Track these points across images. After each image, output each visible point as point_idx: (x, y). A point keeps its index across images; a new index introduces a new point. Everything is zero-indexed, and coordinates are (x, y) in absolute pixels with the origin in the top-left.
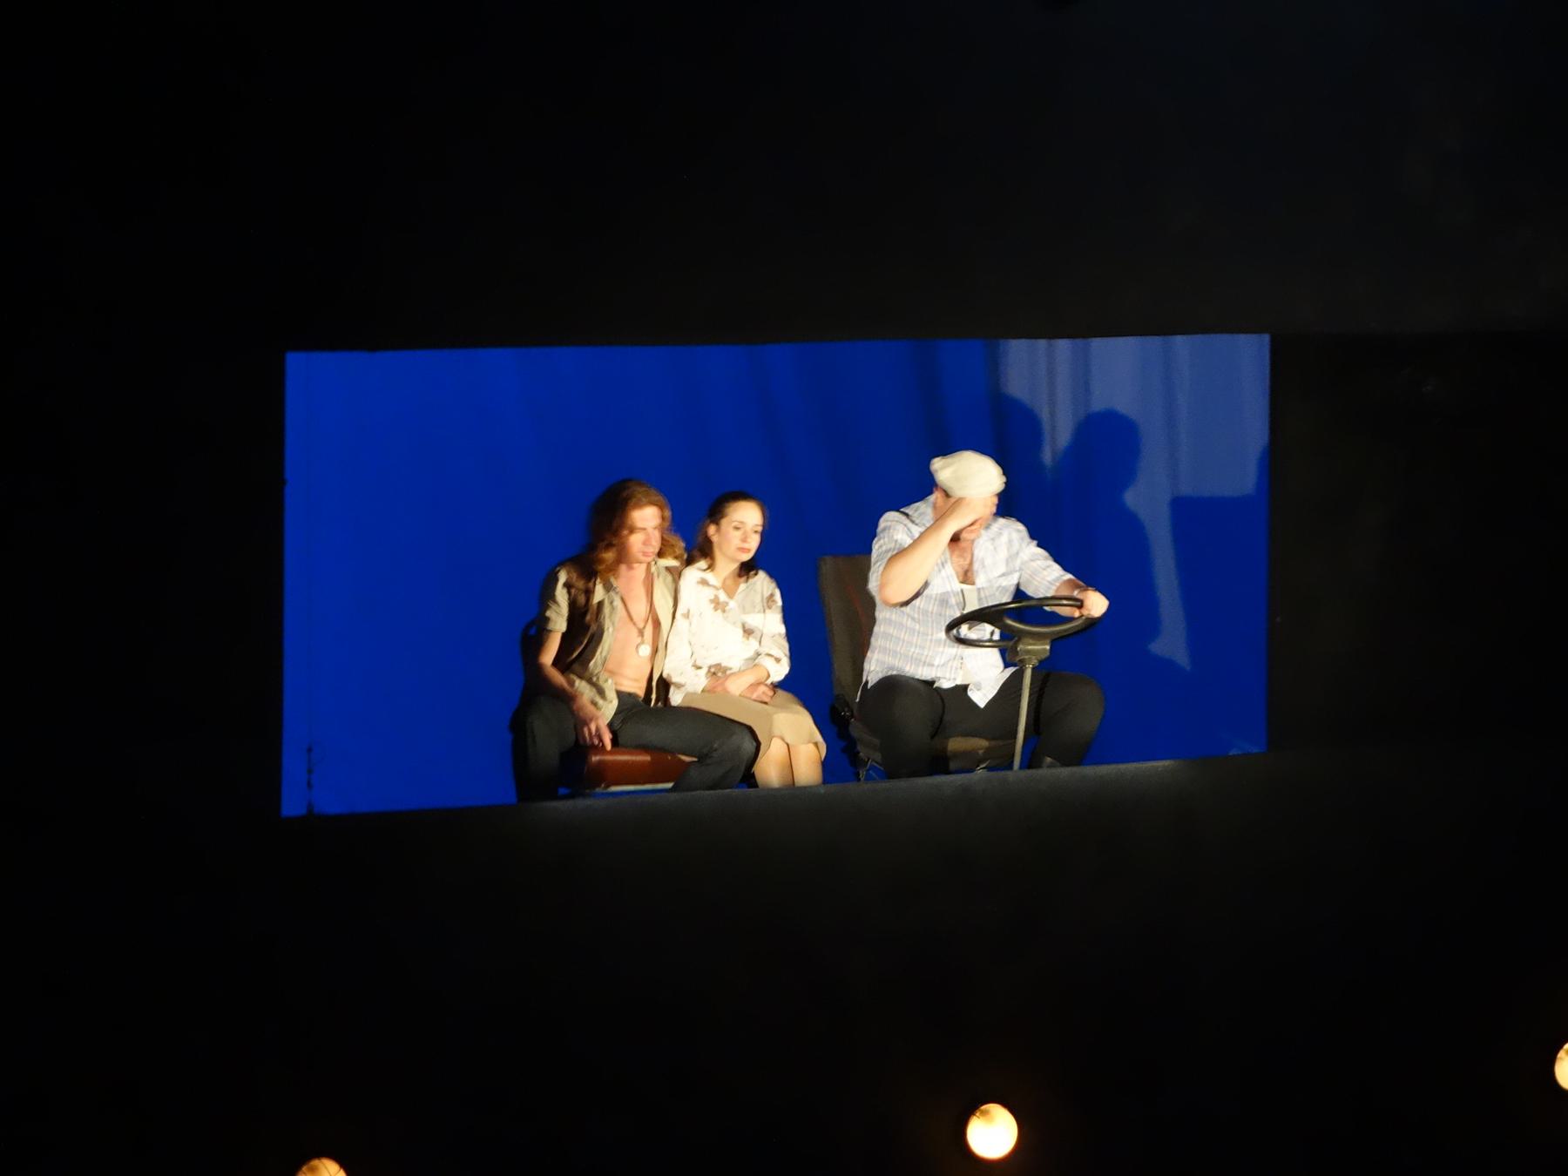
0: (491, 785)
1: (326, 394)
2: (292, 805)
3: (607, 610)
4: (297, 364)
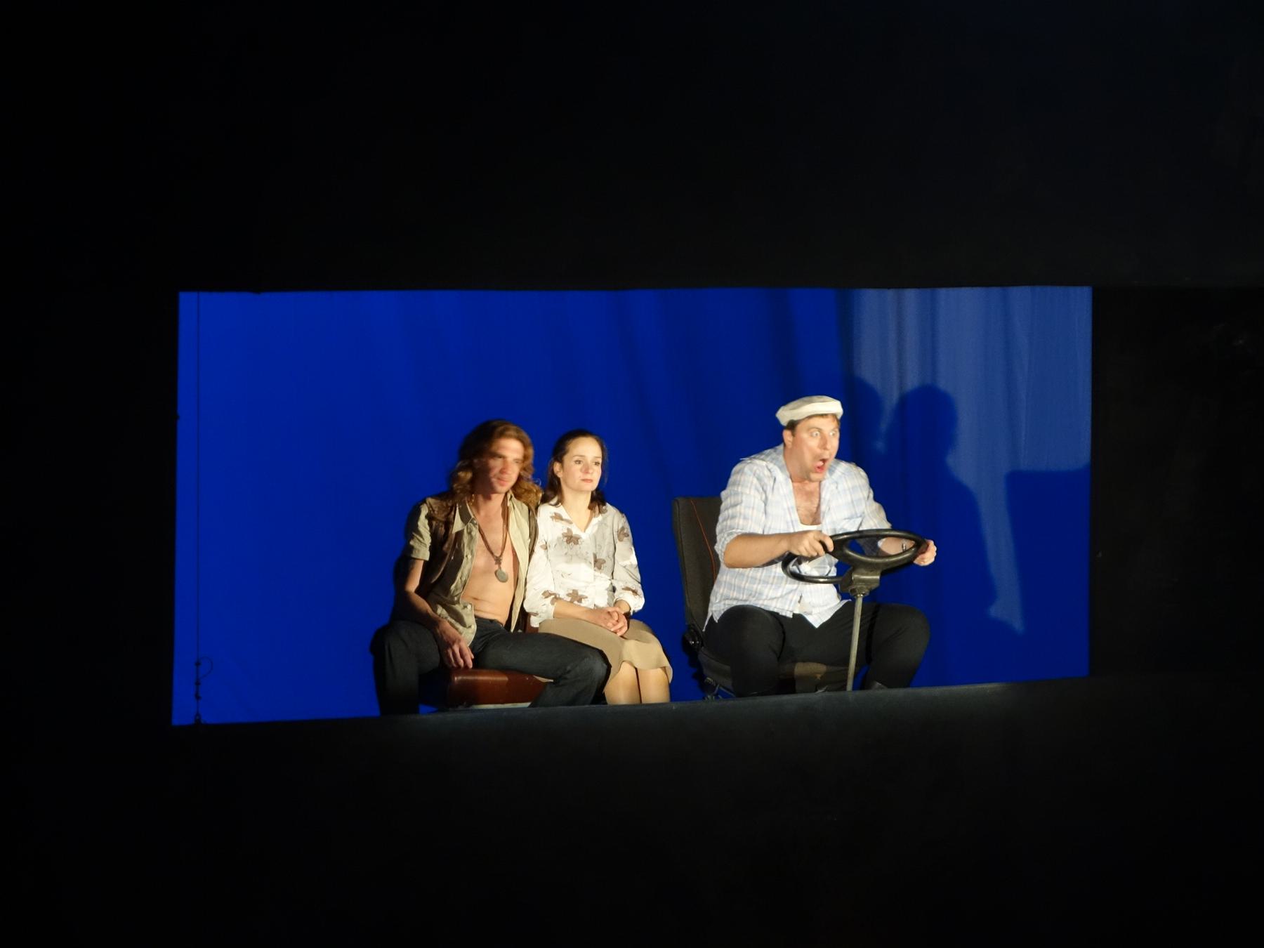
0: (358, 701)
1: (218, 331)
2: (183, 712)
3: (466, 539)
4: (188, 301)
